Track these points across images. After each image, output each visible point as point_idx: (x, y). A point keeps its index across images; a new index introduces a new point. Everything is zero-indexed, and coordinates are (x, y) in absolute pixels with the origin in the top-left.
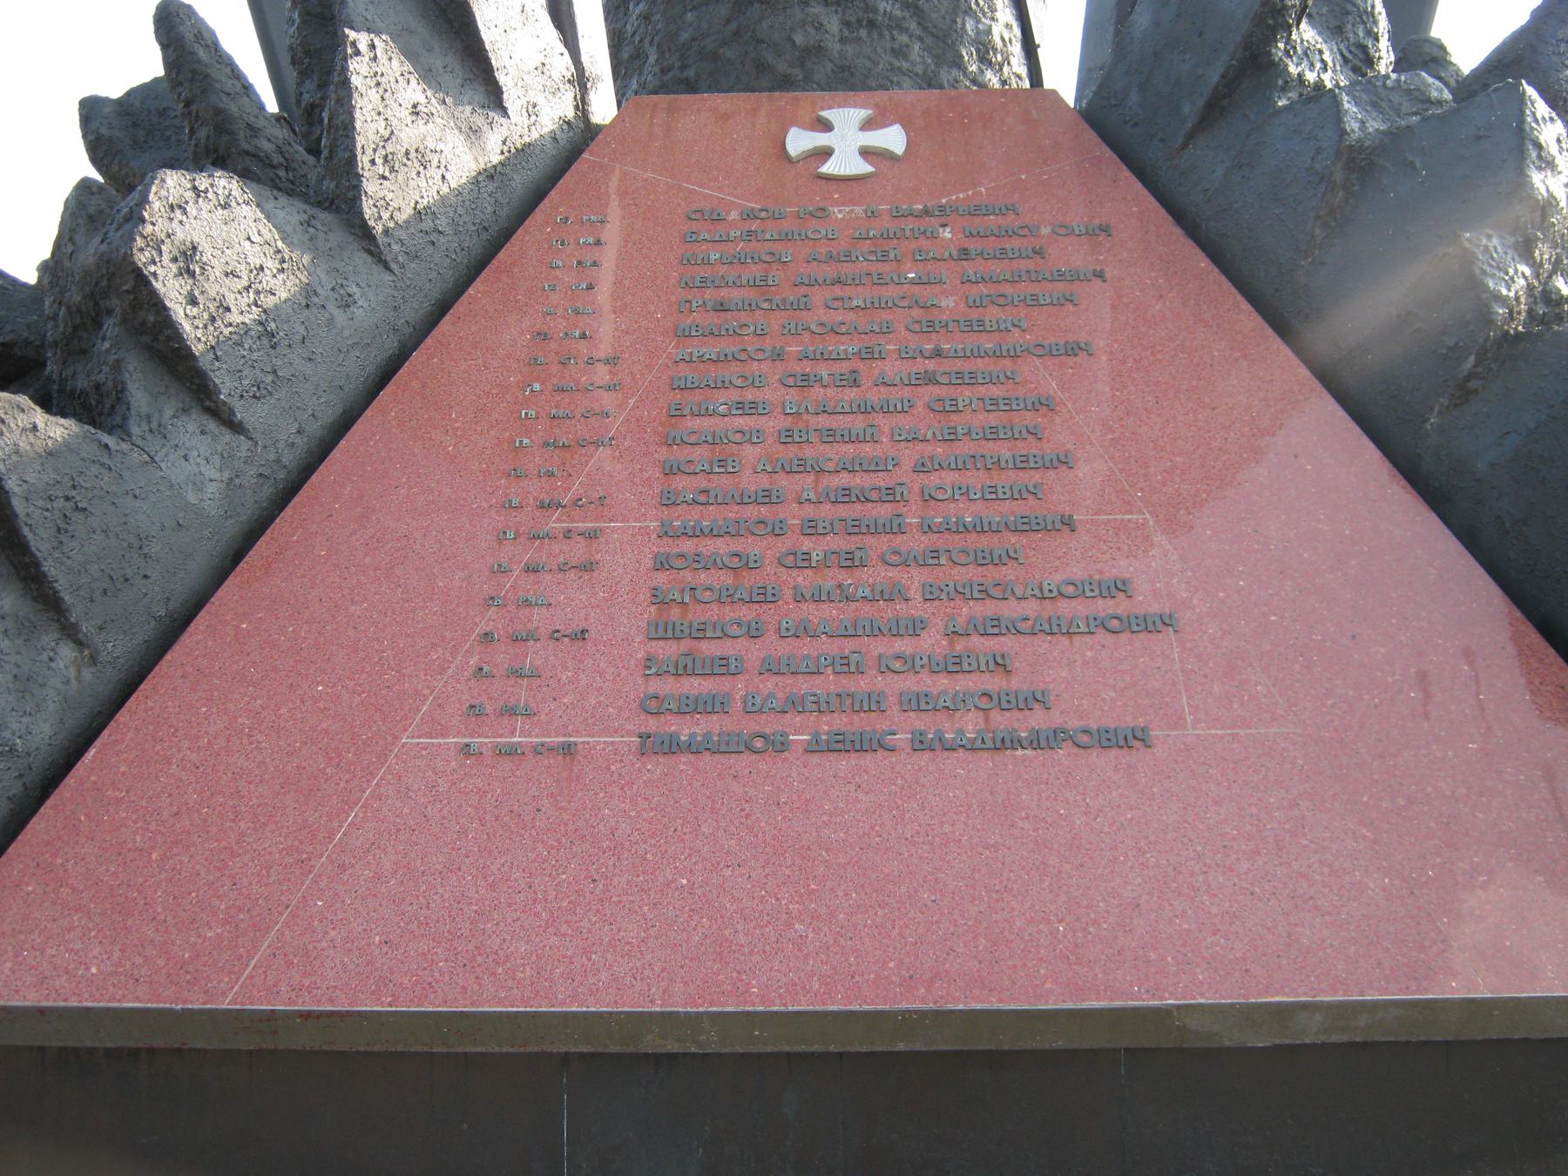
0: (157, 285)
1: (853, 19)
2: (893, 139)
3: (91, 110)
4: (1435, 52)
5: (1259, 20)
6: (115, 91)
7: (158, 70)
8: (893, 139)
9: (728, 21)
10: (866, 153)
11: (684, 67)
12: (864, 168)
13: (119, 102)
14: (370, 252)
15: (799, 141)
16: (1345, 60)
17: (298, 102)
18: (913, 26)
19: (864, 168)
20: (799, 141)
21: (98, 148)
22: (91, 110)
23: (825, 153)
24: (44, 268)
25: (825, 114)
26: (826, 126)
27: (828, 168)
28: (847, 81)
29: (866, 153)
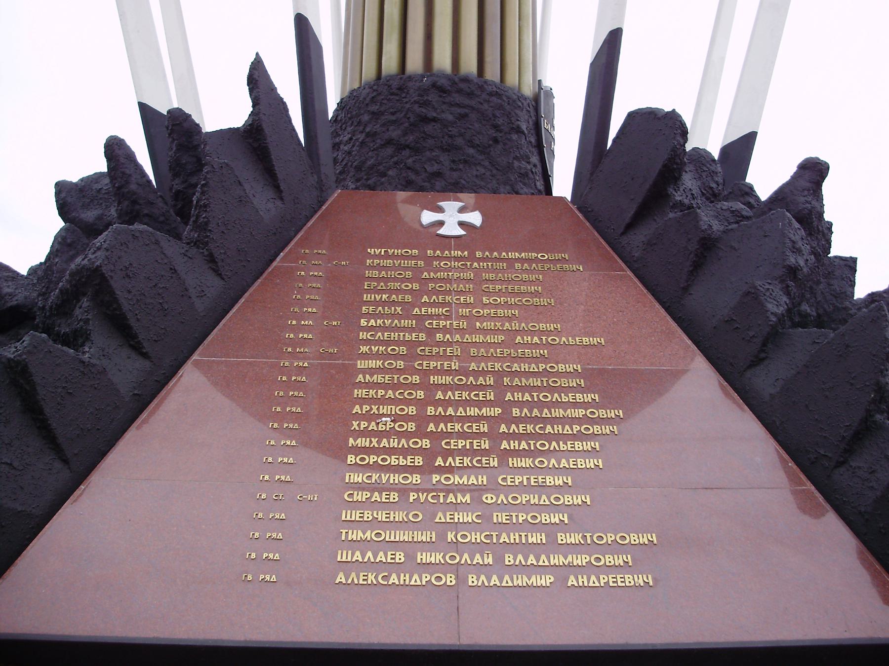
0: (112, 283)
1: (456, 159)
2: (475, 218)
3: (62, 189)
4: (747, 190)
5: (661, 174)
6: (74, 178)
7: (105, 169)
8: (475, 218)
9: (392, 157)
10: (462, 224)
11: (367, 179)
12: (461, 232)
13: (76, 184)
14: (213, 270)
15: (428, 217)
16: (703, 194)
17: (171, 189)
18: (487, 163)
19: (461, 232)
20: (428, 217)
21: (64, 209)
22: (62, 189)
23: (441, 223)
24: (33, 271)
25: (441, 204)
26: (441, 210)
27: (442, 231)
28: (454, 188)
29: (462, 224)
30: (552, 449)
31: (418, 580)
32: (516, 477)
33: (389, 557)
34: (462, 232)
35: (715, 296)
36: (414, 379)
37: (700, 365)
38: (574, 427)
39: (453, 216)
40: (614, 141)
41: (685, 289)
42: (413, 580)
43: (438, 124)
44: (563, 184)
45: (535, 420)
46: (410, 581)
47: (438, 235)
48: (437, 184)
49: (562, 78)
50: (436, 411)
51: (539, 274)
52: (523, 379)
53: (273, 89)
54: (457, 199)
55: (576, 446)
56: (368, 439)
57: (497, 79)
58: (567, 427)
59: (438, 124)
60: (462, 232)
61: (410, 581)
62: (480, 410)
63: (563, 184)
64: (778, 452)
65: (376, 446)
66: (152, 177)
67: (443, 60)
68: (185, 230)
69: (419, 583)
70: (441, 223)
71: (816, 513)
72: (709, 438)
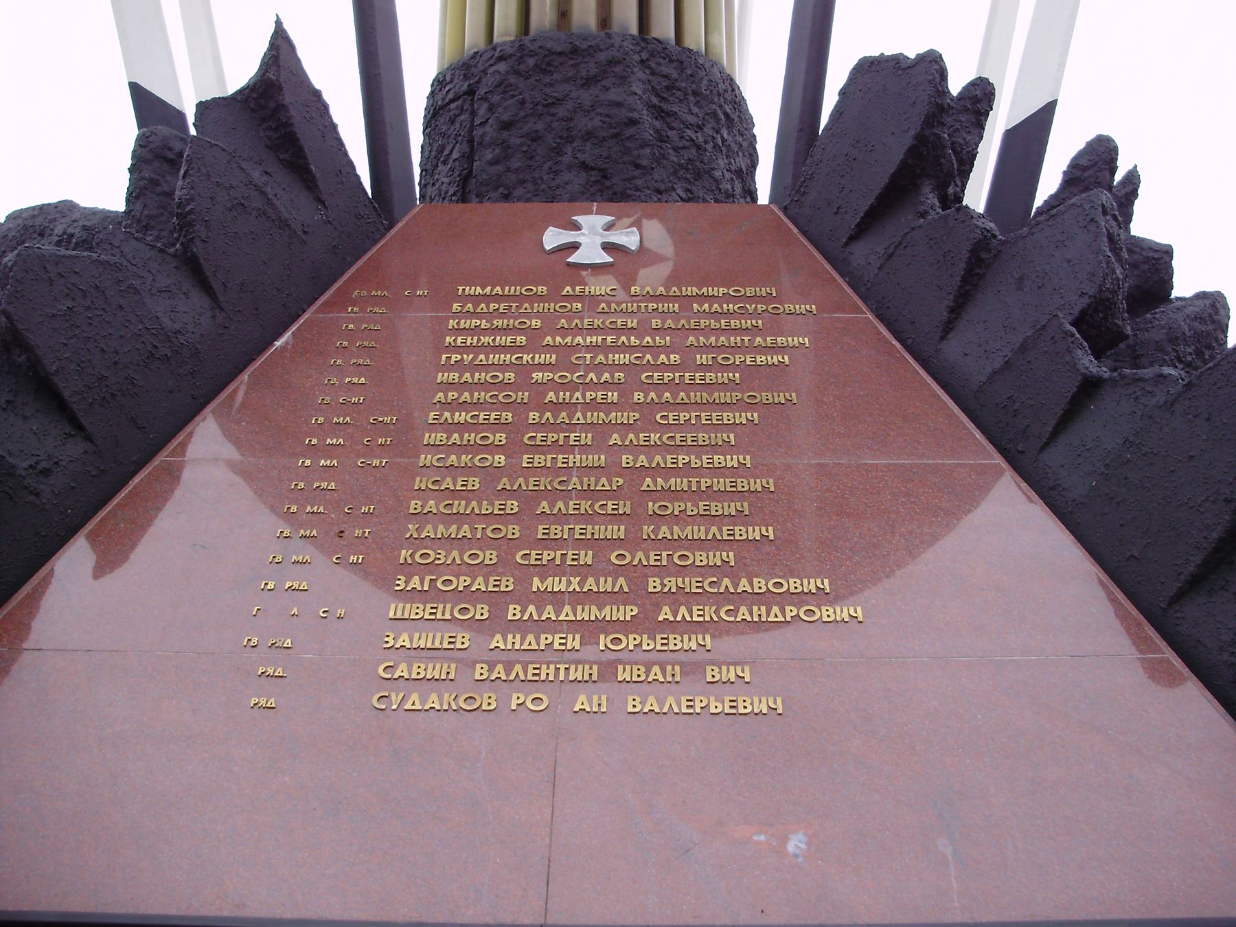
2: (629, 239)
10: (608, 247)
15: (553, 238)
20: (553, 238)
23: (574, 247)
26: (577, 227)
29: (608, 247)
34: (608, 259)
35: (978, 345)
38: (788, 608)
39: (592, 234)
42: (772, 614)
43: (584, 110)
44: (763, 197)
45: (721, 598)
46: (768, 616)
47: (569, 264)
49: (762, 84)
50: (523, 612)
51: (757, 319)
52: (675, 528)
54: (628, 216)
56: (564, 579)
58: (775, 609)
59: (584, 110)
60: (608, 259)
61: (768, 616)
62: (600, 610)
63: (763, 197)
65: (578, 590)
70: (574, 247)
71: (1168, 678)
72: (1009, 574)
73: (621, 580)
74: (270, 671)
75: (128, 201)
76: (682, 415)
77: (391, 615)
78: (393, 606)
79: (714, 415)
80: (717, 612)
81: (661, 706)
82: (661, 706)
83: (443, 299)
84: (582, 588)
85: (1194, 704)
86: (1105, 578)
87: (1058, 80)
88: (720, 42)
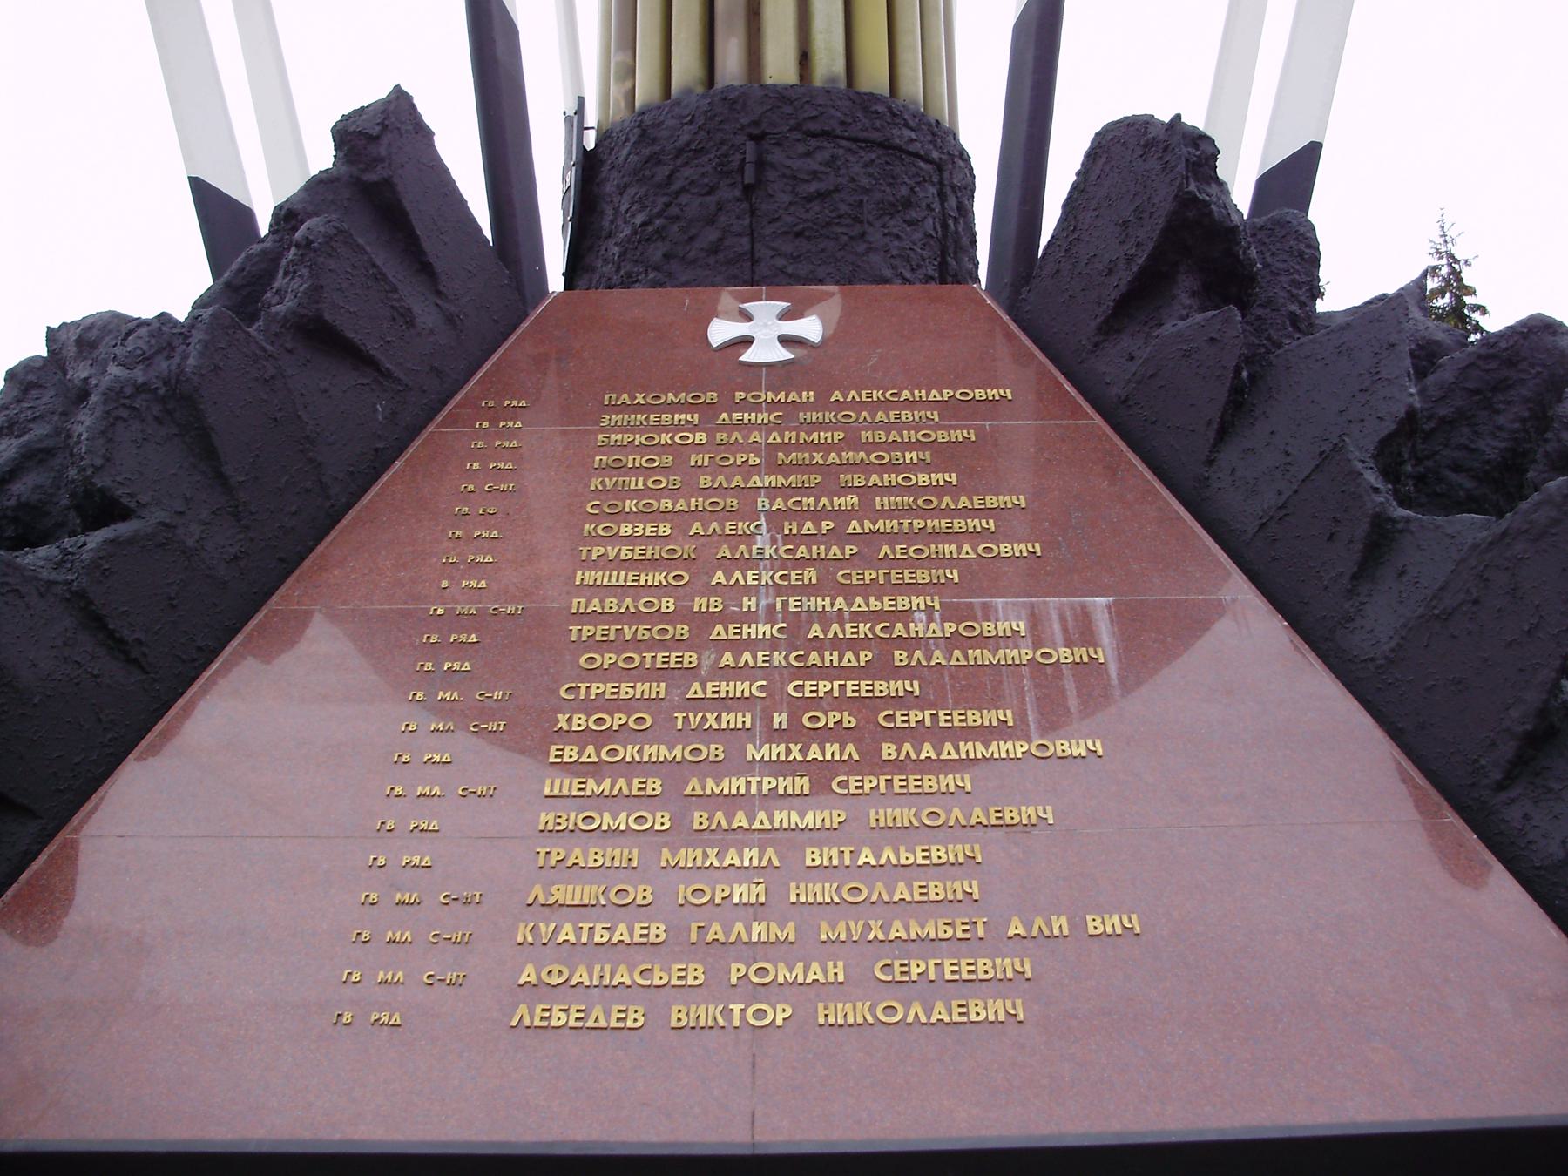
2: (810, 328)
10: (786, 341)
12: (784, 354)
15: (721, 331)
19: (784, 354)
23: (747, 342)
25: (1242, 197)
27: (749, 356)
29: (786, 341)
30: (910, 1019)
31: (766, 821)
32: (912, 713)
33: (637, 932)
36: (679, 631)
37: (1239, 589)
39: (762, 329)
40: (1070, 206)
41: (1210, 462)
43: (771, 171)
48: (753, 271)
53: (1353, 311)
55: (981, 969)
57: (839, 66)
59: (771, 171)
64: (1396, 760)
66: (1044, 240)
67: (780, 67)
68: (344, 334)
69: (767, 826)
70: (747, 342)
71: (1471, 877)
73: (770, 852)
74: (416, 860)
75: (196, 306)
76: (867, 573)
77: (547, 792)
78: (548, 782)
79: (863, 683)
80: (872, 1010)
81: (878, 857)
82: (878, 857)
83: (581, 412)
84: (721, 861)
85: (1504, 899)
86: (1396, 752)
87: (1324, 120)
88: (912, 86)
